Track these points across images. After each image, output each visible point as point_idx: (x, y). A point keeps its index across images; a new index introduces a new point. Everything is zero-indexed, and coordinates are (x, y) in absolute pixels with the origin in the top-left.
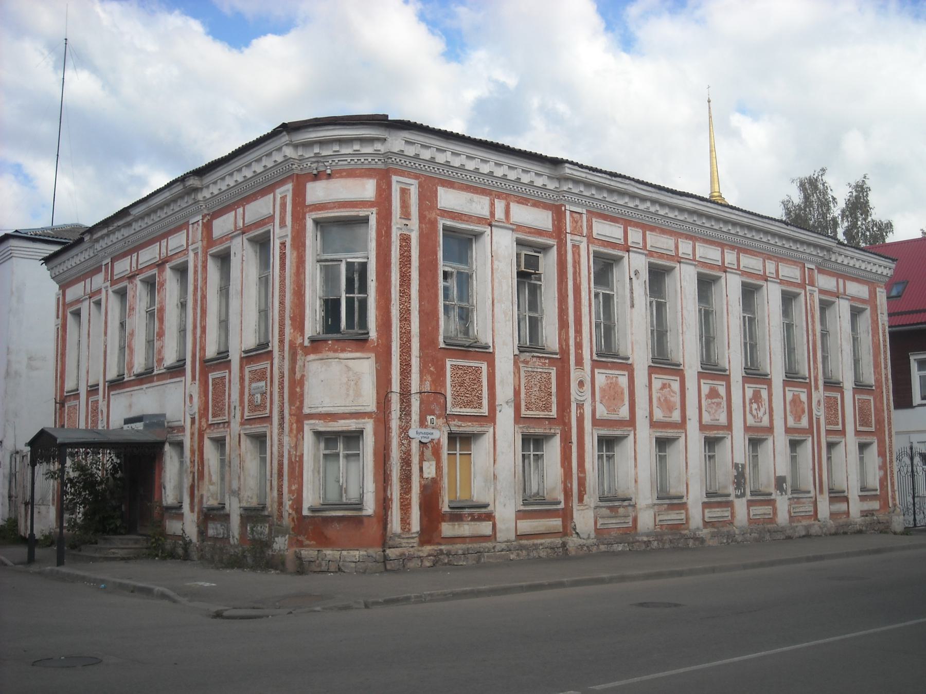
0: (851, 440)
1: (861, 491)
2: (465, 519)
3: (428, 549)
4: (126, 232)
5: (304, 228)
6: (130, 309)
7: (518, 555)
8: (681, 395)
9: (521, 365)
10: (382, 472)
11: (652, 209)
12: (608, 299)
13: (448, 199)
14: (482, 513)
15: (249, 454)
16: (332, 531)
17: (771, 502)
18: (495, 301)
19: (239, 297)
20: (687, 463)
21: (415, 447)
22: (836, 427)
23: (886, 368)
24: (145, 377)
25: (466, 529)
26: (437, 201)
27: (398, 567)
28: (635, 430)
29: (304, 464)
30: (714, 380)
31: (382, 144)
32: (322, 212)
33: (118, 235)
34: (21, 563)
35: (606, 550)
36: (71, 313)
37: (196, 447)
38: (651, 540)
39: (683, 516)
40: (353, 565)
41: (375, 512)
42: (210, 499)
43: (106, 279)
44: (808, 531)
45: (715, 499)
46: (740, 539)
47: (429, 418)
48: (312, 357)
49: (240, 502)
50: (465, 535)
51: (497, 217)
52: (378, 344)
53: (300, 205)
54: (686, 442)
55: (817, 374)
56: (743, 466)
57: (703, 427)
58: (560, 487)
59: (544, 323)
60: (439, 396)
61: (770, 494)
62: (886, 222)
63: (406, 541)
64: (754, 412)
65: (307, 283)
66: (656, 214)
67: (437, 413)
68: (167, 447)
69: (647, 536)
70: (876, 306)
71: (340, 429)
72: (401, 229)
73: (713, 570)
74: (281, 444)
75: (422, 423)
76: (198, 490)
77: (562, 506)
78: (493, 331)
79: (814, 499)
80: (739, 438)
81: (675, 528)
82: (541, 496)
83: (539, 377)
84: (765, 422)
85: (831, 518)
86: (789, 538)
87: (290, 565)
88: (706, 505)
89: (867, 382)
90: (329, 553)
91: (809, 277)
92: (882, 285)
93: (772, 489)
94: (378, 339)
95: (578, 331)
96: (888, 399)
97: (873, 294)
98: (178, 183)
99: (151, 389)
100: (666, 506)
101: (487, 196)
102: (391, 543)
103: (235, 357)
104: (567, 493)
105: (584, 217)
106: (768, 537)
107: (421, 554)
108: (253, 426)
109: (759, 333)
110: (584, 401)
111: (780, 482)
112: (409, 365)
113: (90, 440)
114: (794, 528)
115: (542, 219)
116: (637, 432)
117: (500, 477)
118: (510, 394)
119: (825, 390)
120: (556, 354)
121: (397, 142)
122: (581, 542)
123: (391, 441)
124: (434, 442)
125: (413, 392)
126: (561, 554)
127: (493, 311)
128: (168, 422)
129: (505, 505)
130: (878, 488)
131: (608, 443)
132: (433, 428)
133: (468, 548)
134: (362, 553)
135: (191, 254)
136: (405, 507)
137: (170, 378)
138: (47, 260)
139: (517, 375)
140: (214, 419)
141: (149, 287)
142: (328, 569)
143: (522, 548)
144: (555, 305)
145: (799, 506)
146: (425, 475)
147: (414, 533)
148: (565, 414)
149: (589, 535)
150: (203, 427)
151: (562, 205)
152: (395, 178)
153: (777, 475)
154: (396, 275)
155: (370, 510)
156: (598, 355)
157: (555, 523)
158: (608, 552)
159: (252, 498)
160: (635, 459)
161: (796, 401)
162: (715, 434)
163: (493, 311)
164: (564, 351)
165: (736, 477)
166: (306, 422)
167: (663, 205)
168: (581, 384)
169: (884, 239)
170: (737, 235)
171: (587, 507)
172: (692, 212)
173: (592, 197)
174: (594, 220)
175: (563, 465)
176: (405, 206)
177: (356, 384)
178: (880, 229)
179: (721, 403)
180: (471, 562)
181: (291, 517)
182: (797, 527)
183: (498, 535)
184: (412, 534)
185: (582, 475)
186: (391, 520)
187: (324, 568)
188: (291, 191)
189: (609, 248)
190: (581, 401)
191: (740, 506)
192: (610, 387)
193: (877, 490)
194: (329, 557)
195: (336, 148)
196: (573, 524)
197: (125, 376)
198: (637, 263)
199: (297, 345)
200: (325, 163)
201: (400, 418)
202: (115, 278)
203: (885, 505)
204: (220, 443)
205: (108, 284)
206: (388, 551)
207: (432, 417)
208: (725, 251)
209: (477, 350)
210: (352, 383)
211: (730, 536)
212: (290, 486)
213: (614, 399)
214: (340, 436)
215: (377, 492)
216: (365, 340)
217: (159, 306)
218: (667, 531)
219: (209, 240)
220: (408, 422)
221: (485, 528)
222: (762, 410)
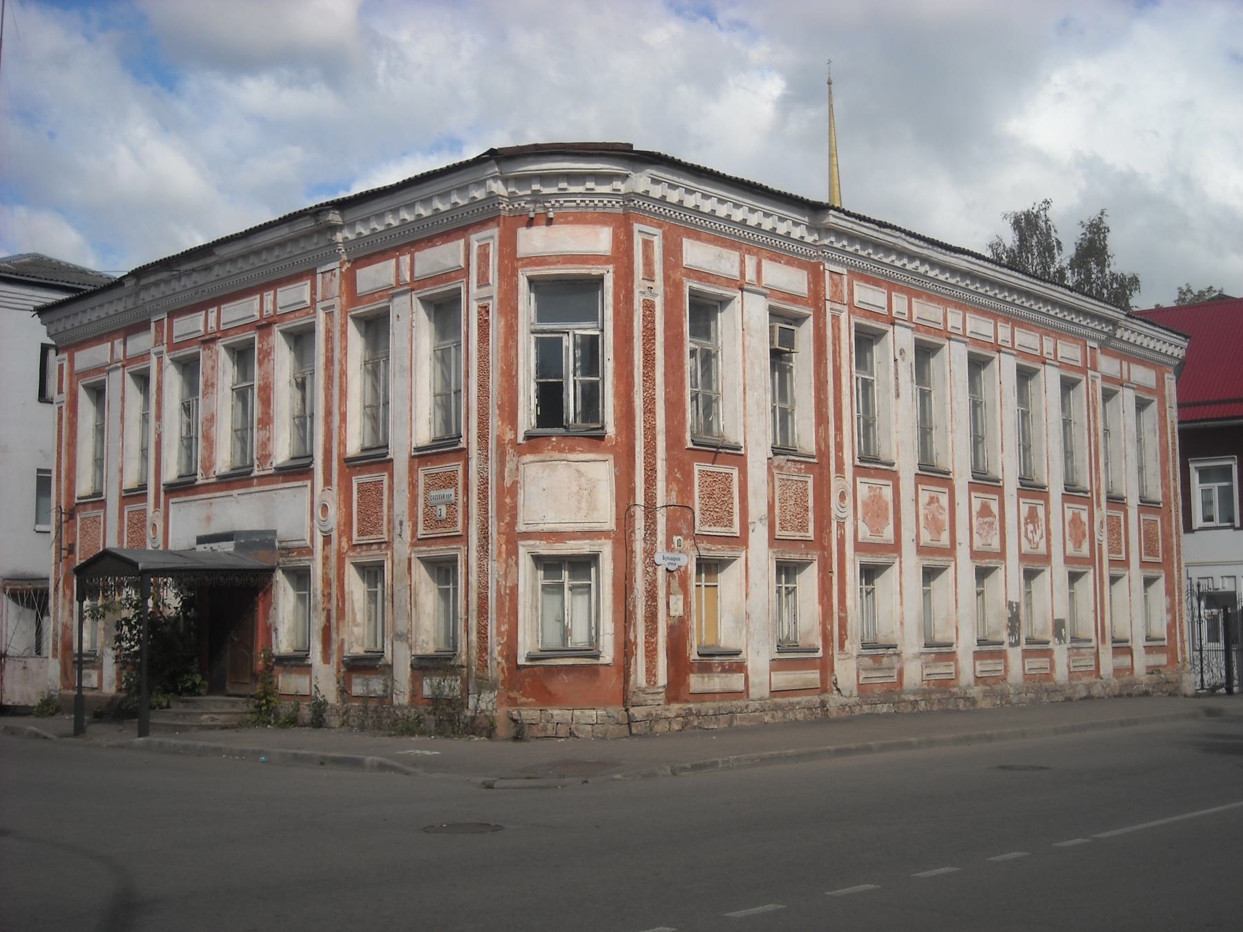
0: (1136, 573)
1: (1147, 640)
2: (714, 670)
3: (675, 708)
4: (199, 278)
5: (514, 289)
6: (206, 385)
7: (773, 717)
8: (950, 512)
9: (775, 471)
10: (622, 609)
11: (922, 270)
12: (867, 385)
13: (696, 254)
14: (732, 662)
15: (423, 585)
16: (558, 685)
17: (1048, 653)
18: (747, 388)
19: (407, 374)
20: (956, 600)
21: (661, 573)
22: (1119, 556)
23: (1175, 479)
24: (238, 479)
25: (716, 682)
26: (682, 256)
27: (645, 730)
28: (901, 557)
29: (520, 597)
30: (987, 493)
31: (623, 183)
32: (542, 268)
33: (187, 282)
34: (67, 736)
35: (870, 711)
36: (84, 386)
37: (333, 574)
38: (918, 699)
39: (953, 670)
40: (589, 728)
41: (614, 660)
42: (354, 644)
43: (158, 342)
44: (1090, 692)
45: (987, 649)
46: (1014, 700)
47: (676, 538)
48: (528, 458)
49: (411, 648)
50: (715, 691)
51: (748, 278)
52: (617, 443)
53: (510, 260)
54: (956, 573)
55: (1099, 485)
56: (1018, 605)
57: (975, 555)
58: (818, 629)
59: (795, 417)
60: (686, 510)
61: (1047, 643)
62: (1130, 276)
63: (651, 697)
64: (1030, 535)
65: (521, 360)
66: (925, 276)
67: (685, 532)
68: (279, 576)
69: (914, 694)
70: (1164, 397)
71: (569, 552)
72: (643, 293)
73: (968, 740)
74: (483, 572)
75: (669, 545)
76: (338, 633)
77: (820, 654)
78: (745, 427)
79: (1095, 650)
80: (1013, 568)
81: (944, 685)
82: (792, 642)
83: (794, 488)
84: (1042, 549)
85: (1114, 675)
86: (1069, 699)
87: (502, 730)
88: (978, 656)
89: (1152, 498)
90: (557, 713)
91: (1091, 359)
92: (1171, 370)
93: (1049, 636)
94: (616, 435)
95: (839, 428)
96: (1177, 521)
97: (1160, 380)
98: (307, 218)
99: (245, 497)
100: (933, 655)
101: (736, 250)
102: (634, 699)
103: (400, 454)
104: (827, 638)
105: (845, 278)
106: (1045, 698)
107: (670, 715)
108: (433, 548)
109: (1033, 433)
110: (845, 518)
111: (1058, 625)
112: (654, 470)
113: (180, 565)
114: (1073, 687)
115: (792, 280)
116: (903, 559)
117: (753, 616)
118: (764, 509)
119: (1108, 508)
120: (813, 457)
121: (642, 179)
122: (844, 700)
123: (634, 569)
124: (682, 569)
125: (658, 505)
126: (820, 716)
127: (744, 400)
128: (280, 542)
129: (758, 653)
130: (1166, 637)
131: (869, 573)
132: (680, 552)
133: (719, 707)
134: (599, 712)
135: (321, 316)
136: (651, 653)
137: (284, 482)
138: (41, 311)
139: (771, 484)
140: (361, 538)
141: (236, 357)
142: (556, 733)
143: (777, 707)
144: (811, 394)
145: (1079, 658)
146: (672, 613)
147: (660, 687)
148: (824, 535)
149: (851, 691)
150: (343, 548)
151: (820, 263)
152: (637, 227)
153: (1055, 618)
154: (639, 354)
155: (608, 657)
156: (861, 460)
157: (812, 676)
158: (872, 714)
159: (427, 643)
160: (901, 594)
161: (1076, 521)
162: (987, 563)
163: (744, 400)
164: (823, 453)
165: (1010, 619)
166: (521, 543)
167: (933, 264)
168: (842, 496)
169: (1127, 300)
170: (1012, 303)
171: (849, 655)
172: (965, 274)
173: (855, 254)
174: (855, 283)
175: (821, 602)
176: (648, 262)
177: (590, 494)
178: (1122, 286)
179: (993, 523)
180: (723, 725)
181: (500, 667)
182: (1077, 685)
183: (751, 690)
184: (658, 688)
185: (843, 615)
186: (636, 670)
187: (550, 732)
188: (496, 238)
189: (872, 320)
190: (842, 518)
191: (1015, 655)
192: (873, 501)
193: (1164, 639)
194: (556, 719)
195: (563, 185)
196: (834, 678)
197: (199, 476)
198: (902, 339)
199: (506, 442)
200: (546, 204)
201: (645, 539)
202: (175, 341)
203: (1173, 659)
204: (372, 573)
205: (164, 348)
206: (632, 710)
207: (679, 537)
208: (999, 324)
209: (728, 451)
210: (586, 493)
211: (1004, 695)
212: (498, 628)
213: (878, 516)
214: (564, 562)
215: (616, 634)
216: (601, 438)
217: (262, 383)
218: (934, 688)
219: (353, 298)
220: (654, 543)
221: (736, 682)
222: (1039, 532)
